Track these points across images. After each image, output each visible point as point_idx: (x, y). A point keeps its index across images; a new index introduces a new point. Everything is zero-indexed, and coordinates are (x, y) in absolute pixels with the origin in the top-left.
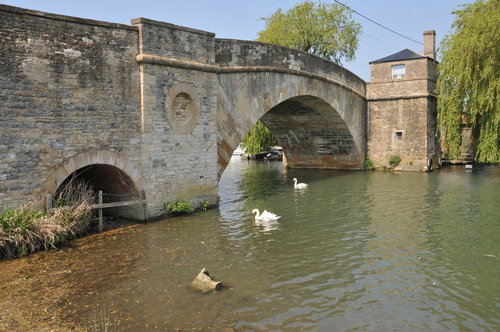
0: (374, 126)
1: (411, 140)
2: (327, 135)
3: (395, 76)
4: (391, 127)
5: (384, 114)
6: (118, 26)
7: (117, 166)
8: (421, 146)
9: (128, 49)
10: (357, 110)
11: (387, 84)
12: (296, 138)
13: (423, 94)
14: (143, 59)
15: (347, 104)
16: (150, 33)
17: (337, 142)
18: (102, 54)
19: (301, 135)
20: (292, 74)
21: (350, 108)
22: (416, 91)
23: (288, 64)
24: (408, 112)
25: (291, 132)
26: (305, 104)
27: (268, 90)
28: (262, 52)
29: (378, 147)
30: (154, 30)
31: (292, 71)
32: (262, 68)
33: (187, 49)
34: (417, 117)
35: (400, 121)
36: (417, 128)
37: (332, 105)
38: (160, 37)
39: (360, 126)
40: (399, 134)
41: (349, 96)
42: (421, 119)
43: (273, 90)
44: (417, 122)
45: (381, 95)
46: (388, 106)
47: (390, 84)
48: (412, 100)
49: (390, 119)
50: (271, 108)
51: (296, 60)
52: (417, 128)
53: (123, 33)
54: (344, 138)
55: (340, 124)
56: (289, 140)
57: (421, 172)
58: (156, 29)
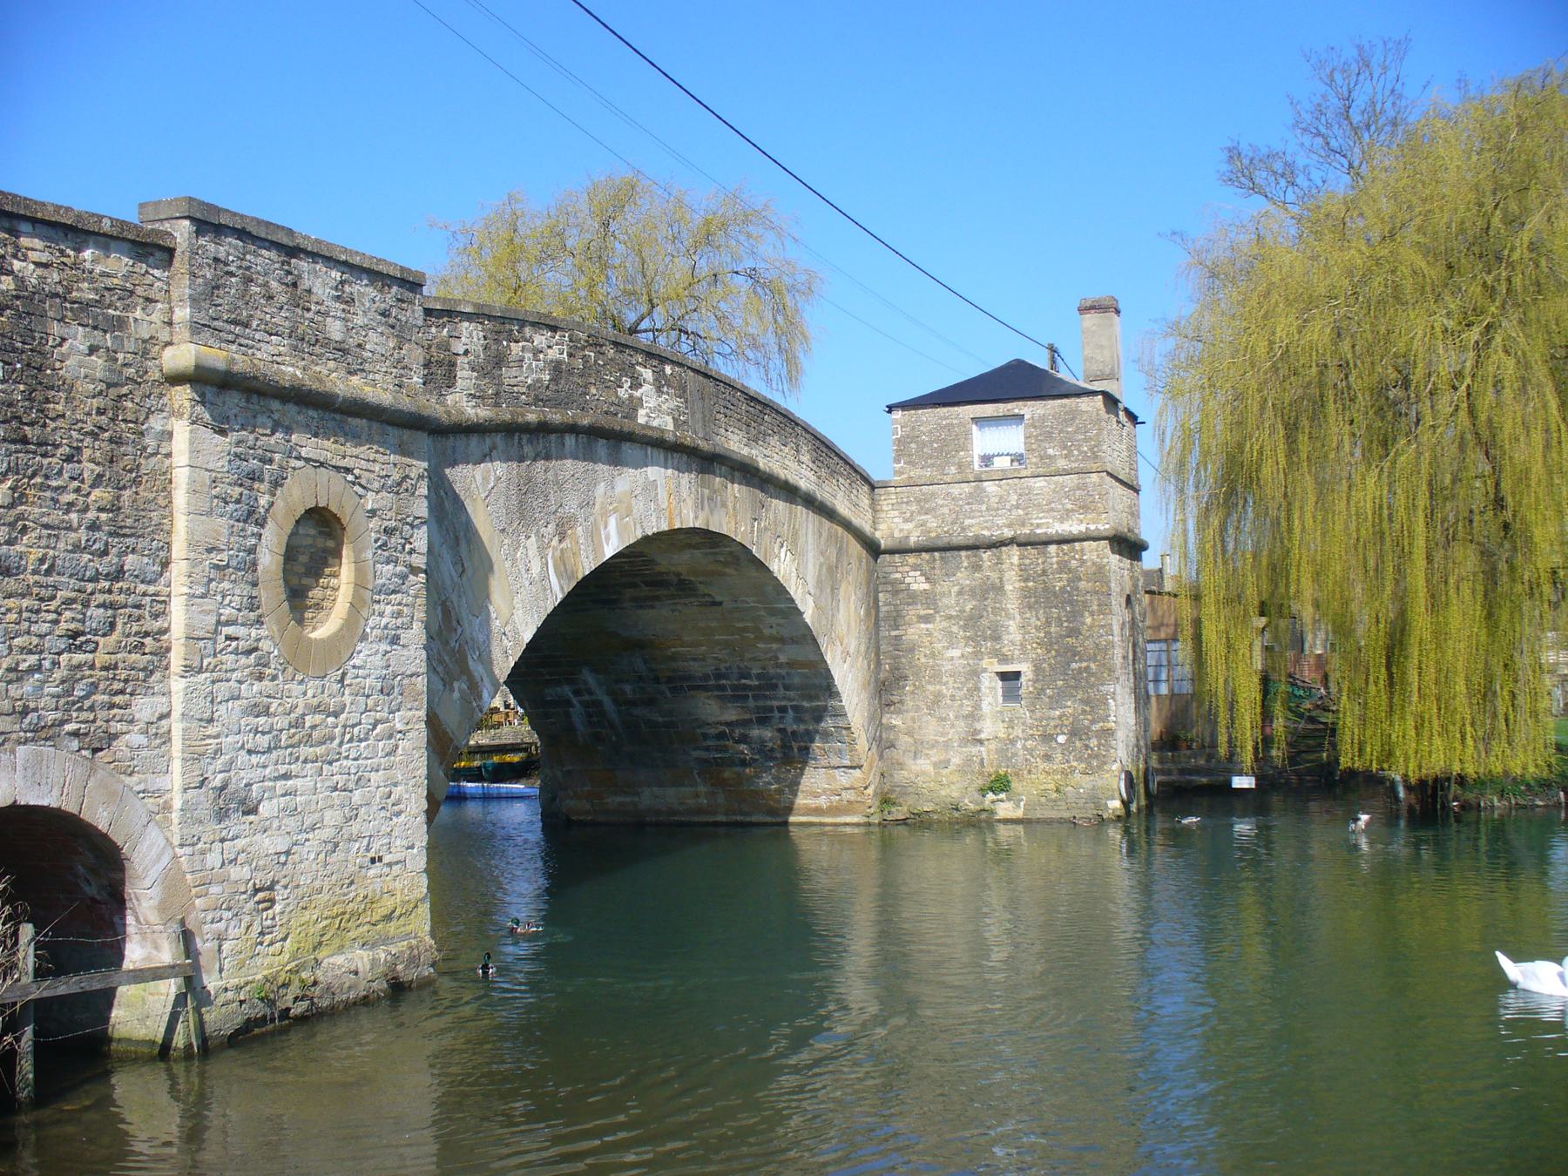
0: (912, 650)
1: (1055, 702)
2: (734, 688)
3: (987, 459)
4: (977, 655)
5: (949, 603)
6: (106, 226)
7: (86, 816)
8: (1093, 722)
9: (136, 320)
10: (851, 588)
11: (956, 490)
12: (607, 701)
13: (1092, 527)
14: (197, 367)
15: (821, 565)
16: (216, 260)
17: (777, 714)
18: (44, 341)
19: (628, 688)
20: (647, 444)
21: (830, 579)
22: (1066, 515)
23: (634, 405)
24: (1039, 596)
25: (589, 678)
26: (680, 562)
27: (571, 506)
28: (553, 354)
29: (930, 729)
30: (229, 248)
31: (650, 433)
32: (555, 417)
33: (335, 330)
34: (1075, 615)
35: (1013, 632)
36: (1074, 653)
37: (774, 567)
38: (248, 280)
39: (863, 648)
40: (1010, 677)
41: (825, 535)
42: (1088, 620)
43: (587, 504)
44: (1074, 632)
45: (935, 527)
46: (963, 575)
47: (966, 488)
48: (1052, 548)
49: (971, 621)
50: (580, 577)
51: (659, 390)
52: (1074, 653)
53: (118, 264)
54: (803, 697)
55: (793, 641)
56: (577, 712)
57: (1102, 821)
58: (236, 248)
